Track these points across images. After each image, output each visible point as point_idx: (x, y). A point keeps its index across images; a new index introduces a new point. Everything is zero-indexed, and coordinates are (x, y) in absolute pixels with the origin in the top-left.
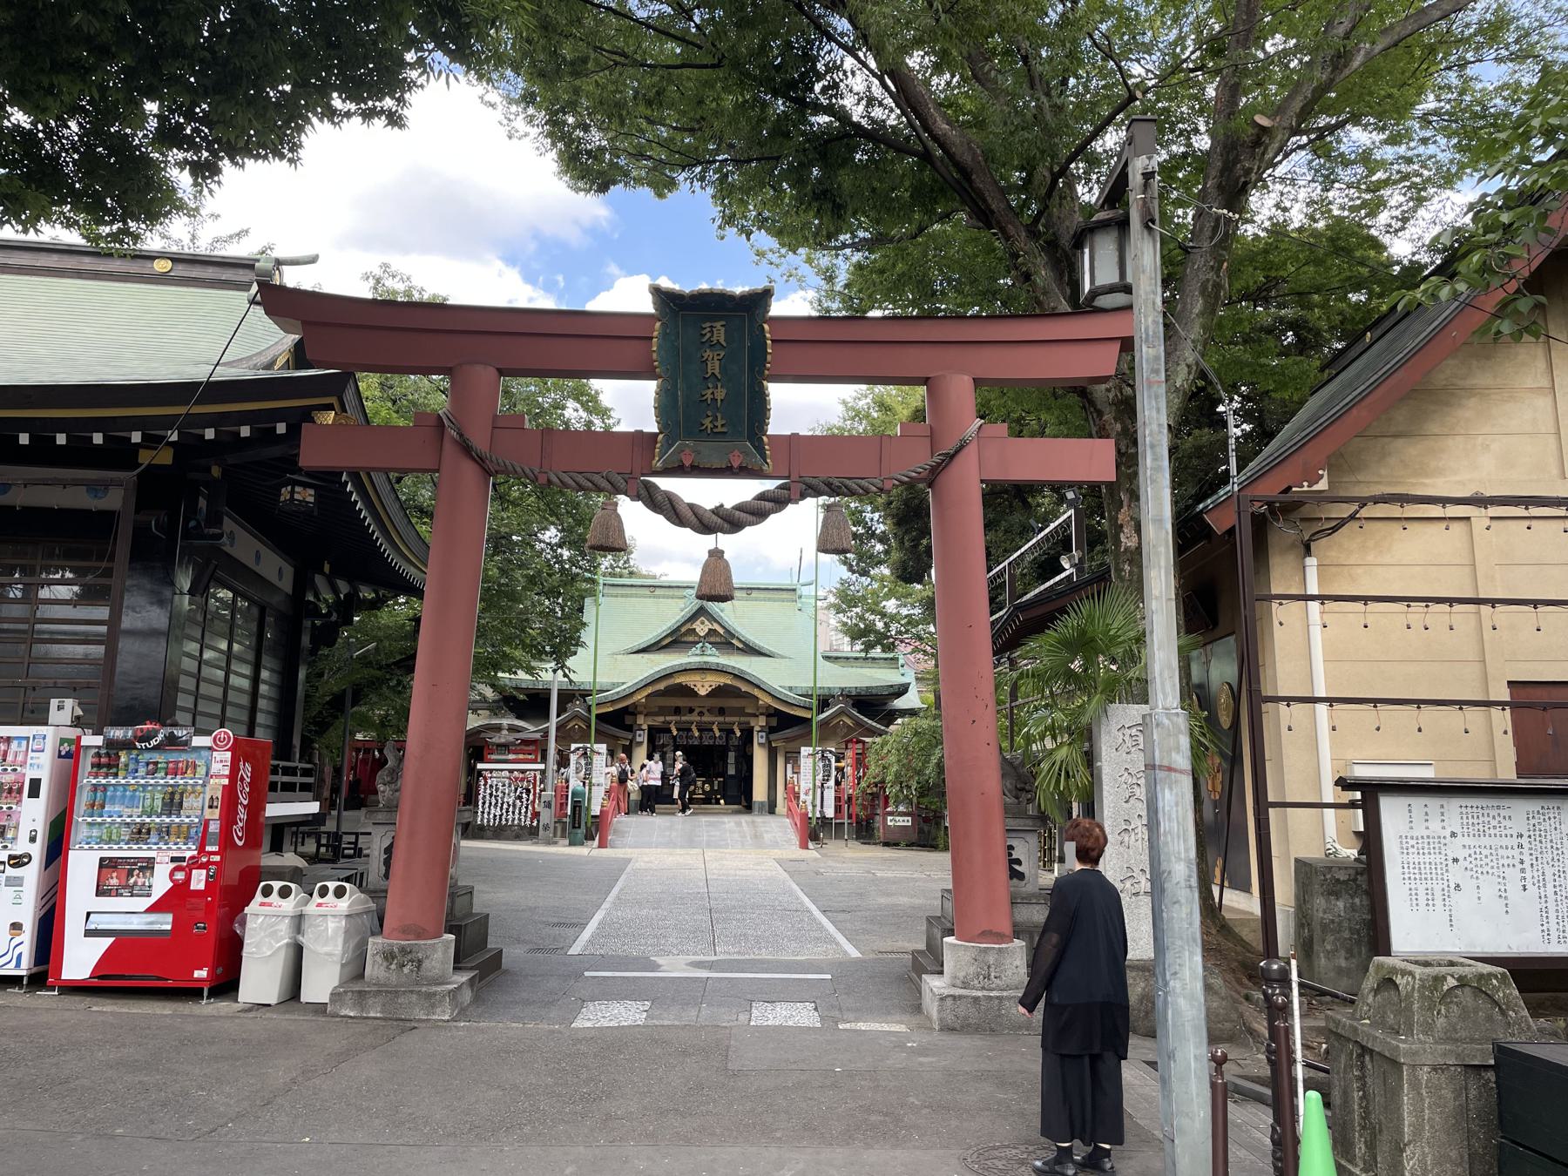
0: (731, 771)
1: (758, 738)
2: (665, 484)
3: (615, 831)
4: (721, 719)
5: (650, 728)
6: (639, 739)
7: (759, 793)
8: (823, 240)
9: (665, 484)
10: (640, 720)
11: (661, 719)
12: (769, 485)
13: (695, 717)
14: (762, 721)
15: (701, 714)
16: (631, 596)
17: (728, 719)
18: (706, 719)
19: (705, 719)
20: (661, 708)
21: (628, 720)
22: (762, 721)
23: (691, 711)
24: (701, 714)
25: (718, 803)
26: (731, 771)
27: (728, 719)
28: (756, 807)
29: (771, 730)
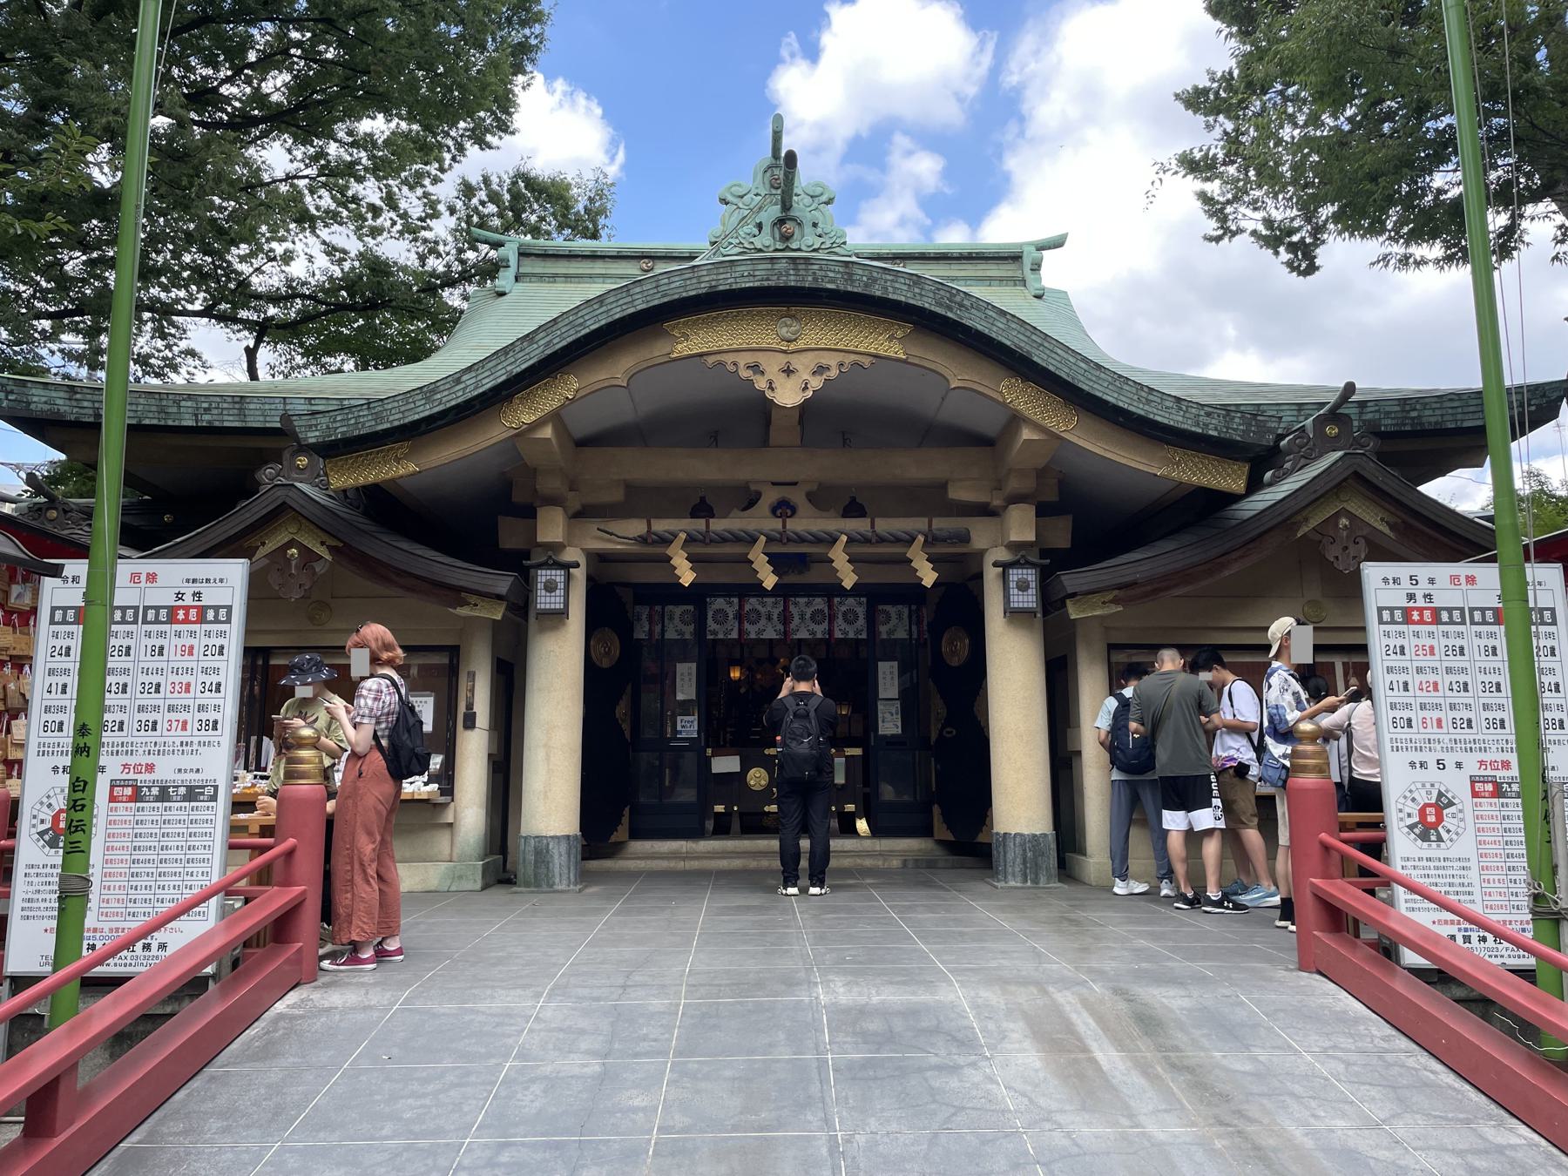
0: (890, 724)
1: (1004, 600)
2: (627, 735)
3: (960, 99)
4: (859, 525)
5: (598, 560)
6: (545, 601)
7: (1019, 801)
8: (827, 15)
9: (627, 735)
10: (552, 527)
11: (636, 527)
12: (629, 687)
13: (761, 521)
14: (1021, 526)
15: (783, 509)
16: (554, 277)
17: (884, 526)
18: (806, 523)
19: (797, 525)
20: (631, 489)
21: (509, 536)
22: (1021, 526)
23: (750, 501)
24: (783, 509)
25: (849, 830)
26: (890, 724)
27: (884, 526)
28: (1012, 858)
29: (1051, 564)
